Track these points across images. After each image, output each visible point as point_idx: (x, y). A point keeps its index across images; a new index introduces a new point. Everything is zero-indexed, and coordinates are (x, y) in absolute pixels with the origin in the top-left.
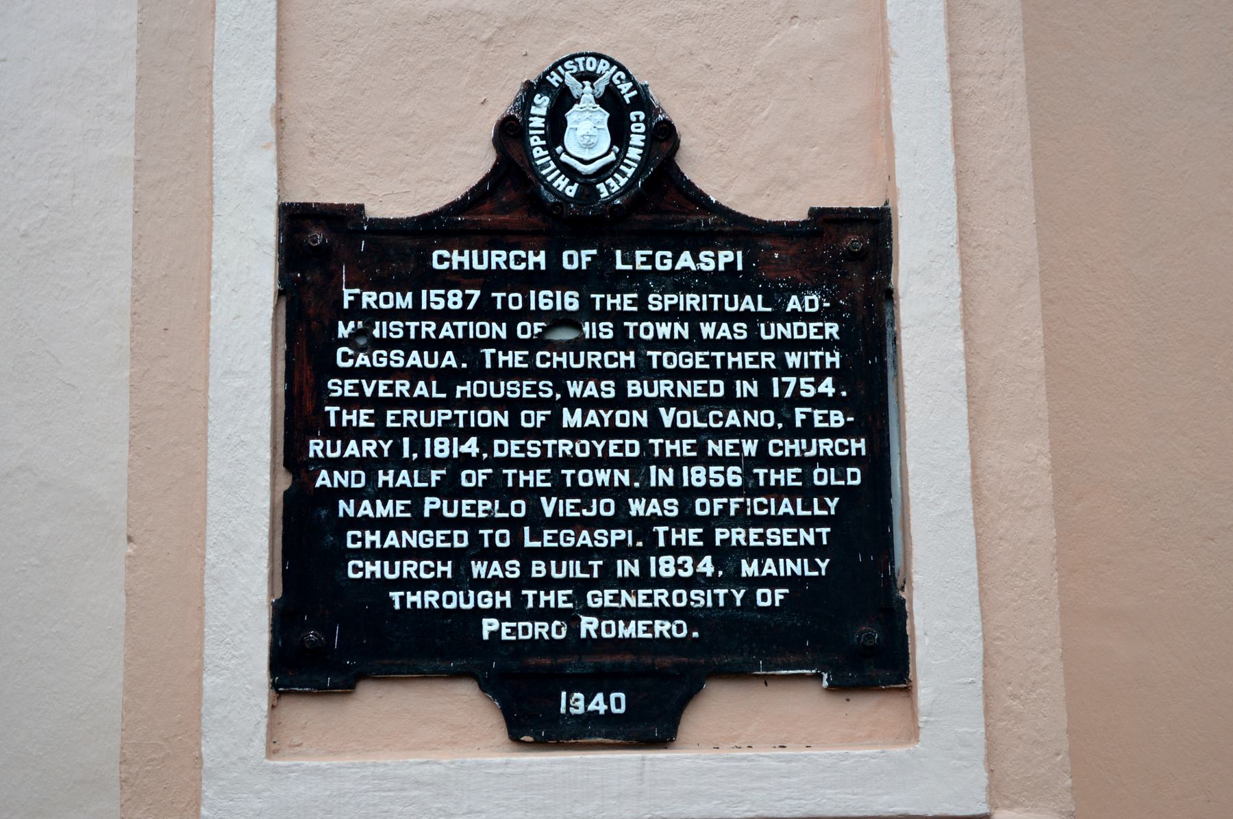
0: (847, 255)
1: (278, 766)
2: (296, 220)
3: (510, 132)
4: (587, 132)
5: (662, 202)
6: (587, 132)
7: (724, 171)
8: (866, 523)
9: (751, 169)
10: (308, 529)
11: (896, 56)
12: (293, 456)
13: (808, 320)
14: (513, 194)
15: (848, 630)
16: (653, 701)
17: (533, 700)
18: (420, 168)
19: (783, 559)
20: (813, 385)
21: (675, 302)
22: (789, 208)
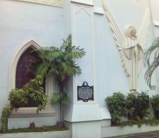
0: (92, 88)
1: (130, 123)
2: (78, 86)
3: (83, 84)
4: (85, 83)
5: (88, 86)
6: (85, 83)
7: (89, 85)
8: (93, 96)
9: (90, 85)
10: (78, 96)
11: (81, 54)
12: (78, 94)
13: (91, 89)
14: (83, 86)
15: (92, 99)
16: (87, 100)
17: (84, 100)
18: (81, 85)
19: (91, 96)
20: (91, 91)
21: (88, 90)
22: (91, 86)
